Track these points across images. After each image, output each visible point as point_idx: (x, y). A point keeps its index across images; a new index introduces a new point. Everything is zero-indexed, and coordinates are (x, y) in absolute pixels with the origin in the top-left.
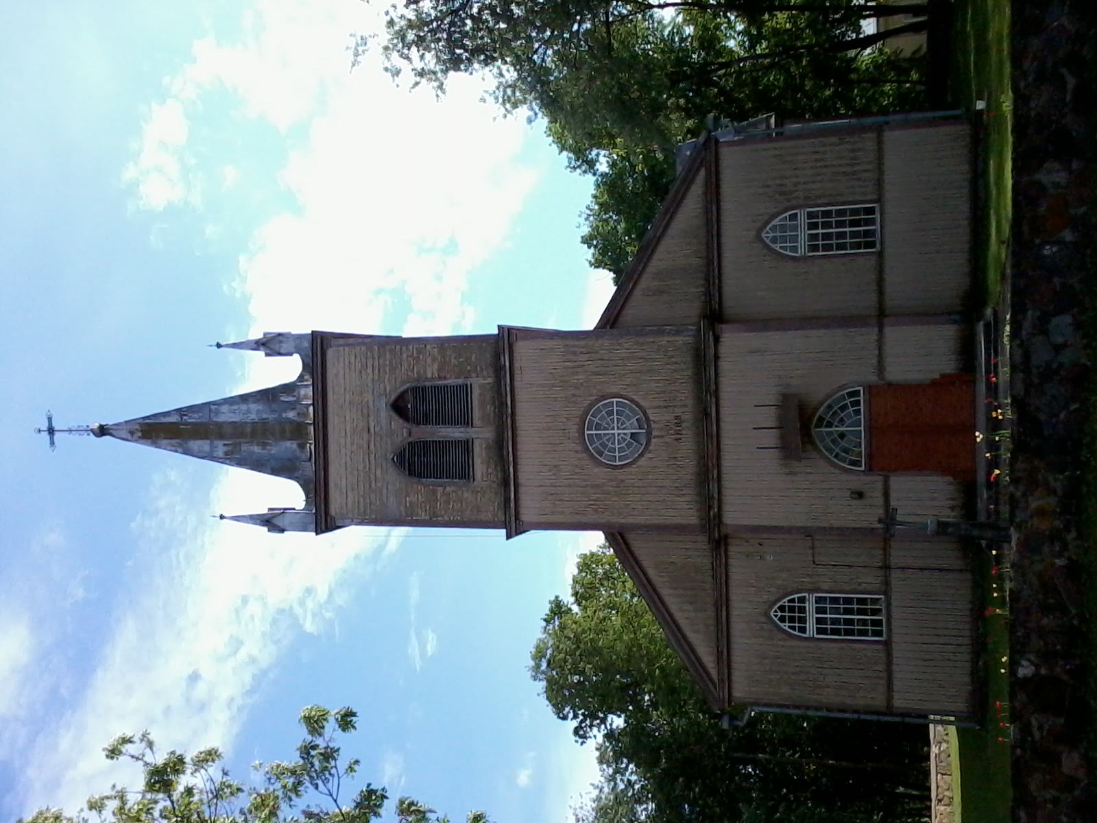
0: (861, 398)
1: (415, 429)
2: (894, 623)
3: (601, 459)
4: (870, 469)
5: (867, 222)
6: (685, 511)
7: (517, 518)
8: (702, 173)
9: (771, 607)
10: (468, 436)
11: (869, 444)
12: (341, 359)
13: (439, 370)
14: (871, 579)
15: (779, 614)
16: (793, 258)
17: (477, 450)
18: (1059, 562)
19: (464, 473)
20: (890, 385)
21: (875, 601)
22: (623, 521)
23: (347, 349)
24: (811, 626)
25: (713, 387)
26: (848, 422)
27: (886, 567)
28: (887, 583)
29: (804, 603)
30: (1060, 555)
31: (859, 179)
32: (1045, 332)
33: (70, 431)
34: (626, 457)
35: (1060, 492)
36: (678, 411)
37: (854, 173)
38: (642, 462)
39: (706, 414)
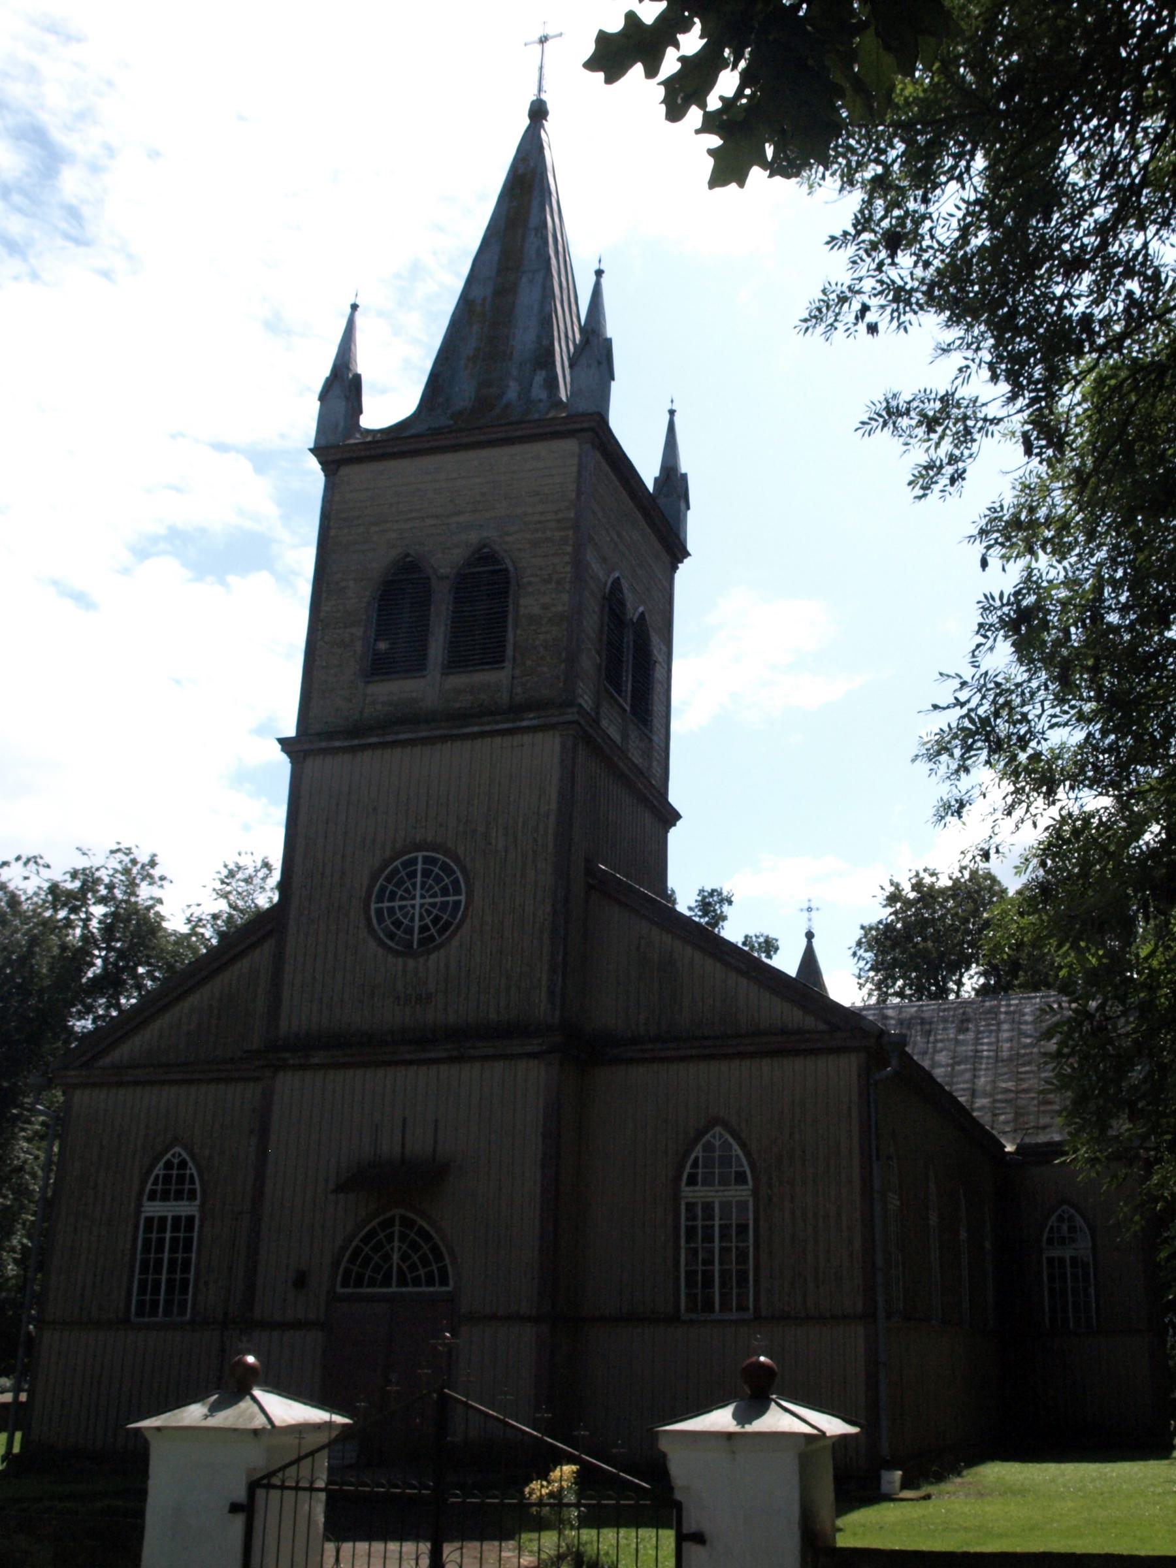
0: (424, 1289)
3: (381, 880)
9: (185, 1148)
16: (678, 1178)
21: (183, 1305)
24: (154, 1209)
26: (404, 1267)
29: (720, 1184)
34: (380, 920)
38: (372, 944)
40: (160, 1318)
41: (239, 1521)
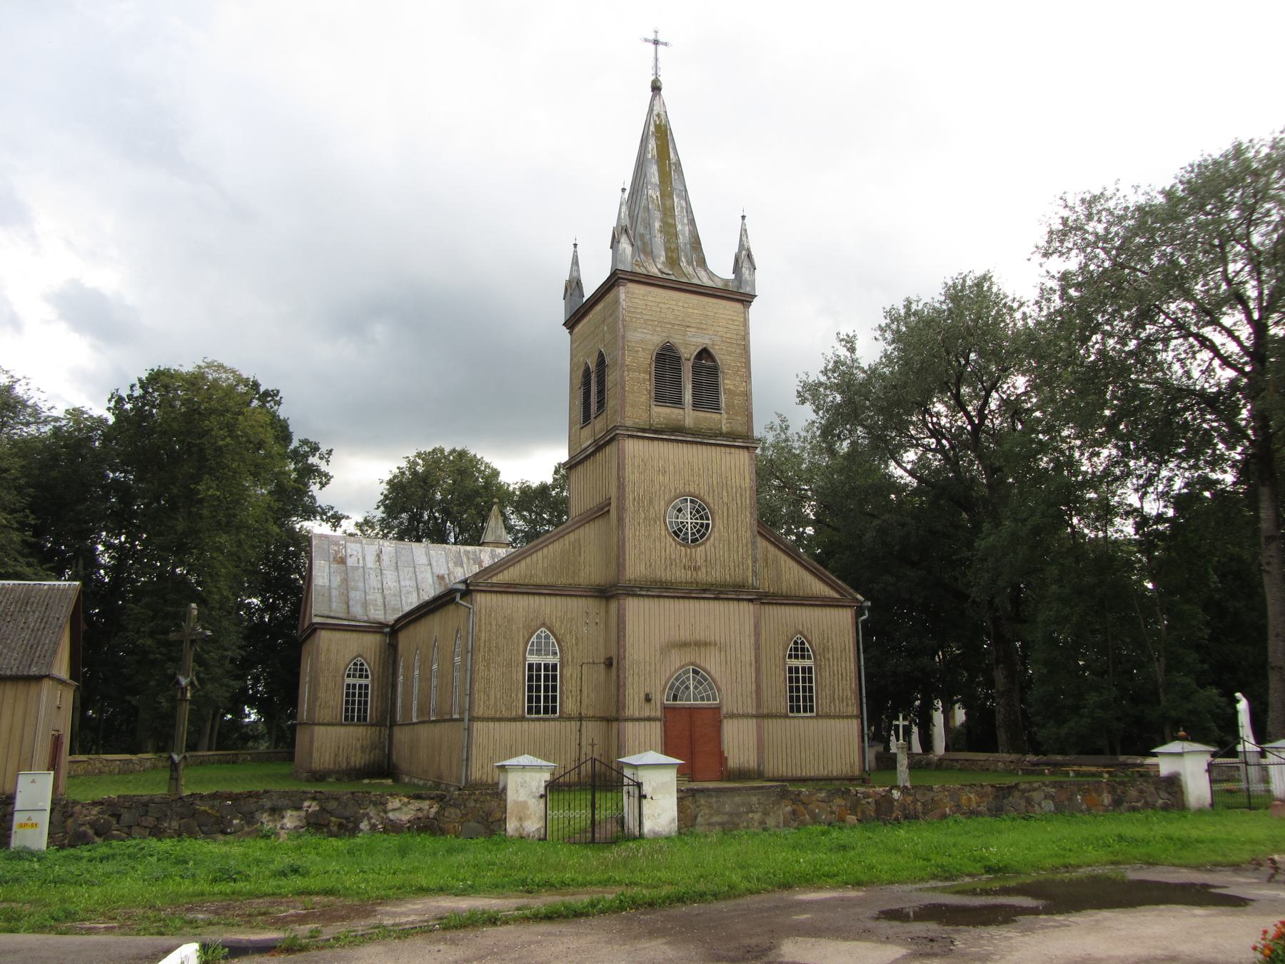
0: (706, 702)
1: (690, 364)
2: (537, 723)
4: (666, 709)
5: (805, 708)
6: (635, 569)
7: (630, 436)
8: (837, 596)
10: (686, 405)
11: (683, 708)
12: (736, 314)
13: (729, 389)
14: (570, 706)
15: (543, 635)
17: (676, 411)
18: (947, 810)
19: (660, 398)
20: (720, 722)
22: (627, 520)
23: (742, 320)
24: (351, 681)
25: (722, 596)
27: (581, 718)
28: (570, 718)
30: (950, 810)
31: (830, 703)
32: (1046, 798)
33: (656, 60)
35: (979, 809)
36: (704, 570)
37: (834, 700)
39: (704, 591)
40: (542, 715)
41: (543, 801)
